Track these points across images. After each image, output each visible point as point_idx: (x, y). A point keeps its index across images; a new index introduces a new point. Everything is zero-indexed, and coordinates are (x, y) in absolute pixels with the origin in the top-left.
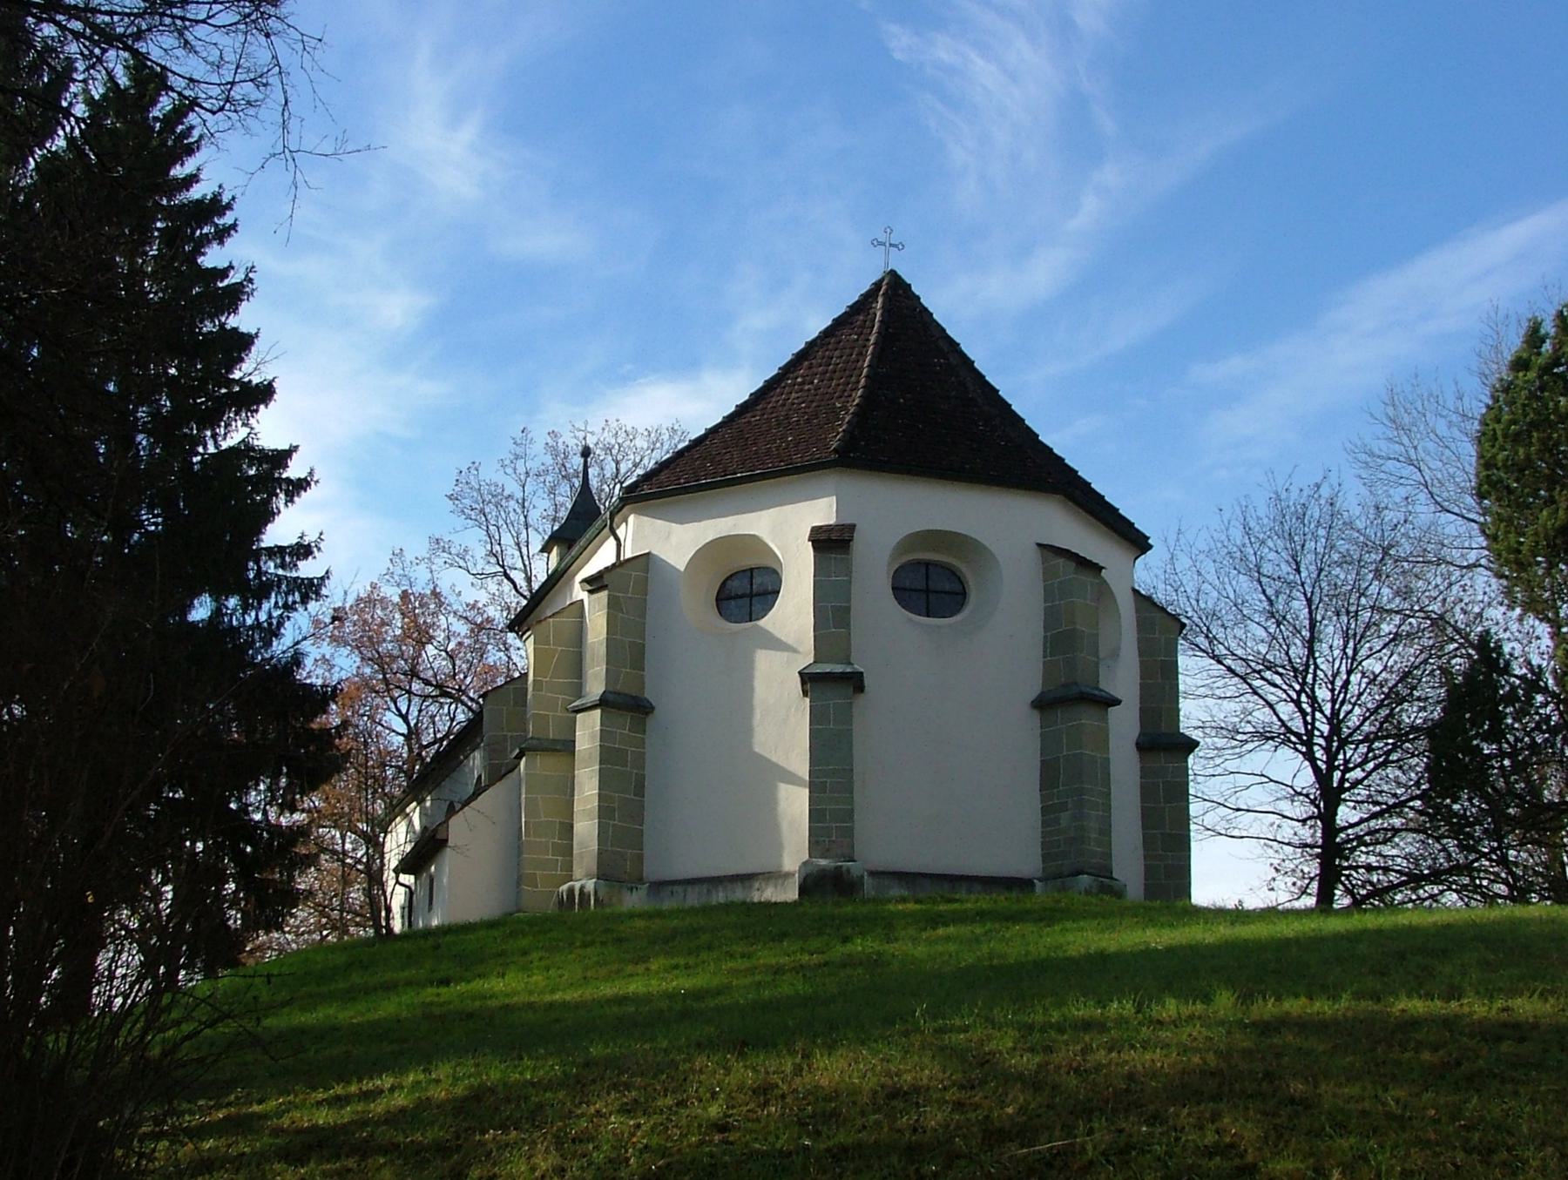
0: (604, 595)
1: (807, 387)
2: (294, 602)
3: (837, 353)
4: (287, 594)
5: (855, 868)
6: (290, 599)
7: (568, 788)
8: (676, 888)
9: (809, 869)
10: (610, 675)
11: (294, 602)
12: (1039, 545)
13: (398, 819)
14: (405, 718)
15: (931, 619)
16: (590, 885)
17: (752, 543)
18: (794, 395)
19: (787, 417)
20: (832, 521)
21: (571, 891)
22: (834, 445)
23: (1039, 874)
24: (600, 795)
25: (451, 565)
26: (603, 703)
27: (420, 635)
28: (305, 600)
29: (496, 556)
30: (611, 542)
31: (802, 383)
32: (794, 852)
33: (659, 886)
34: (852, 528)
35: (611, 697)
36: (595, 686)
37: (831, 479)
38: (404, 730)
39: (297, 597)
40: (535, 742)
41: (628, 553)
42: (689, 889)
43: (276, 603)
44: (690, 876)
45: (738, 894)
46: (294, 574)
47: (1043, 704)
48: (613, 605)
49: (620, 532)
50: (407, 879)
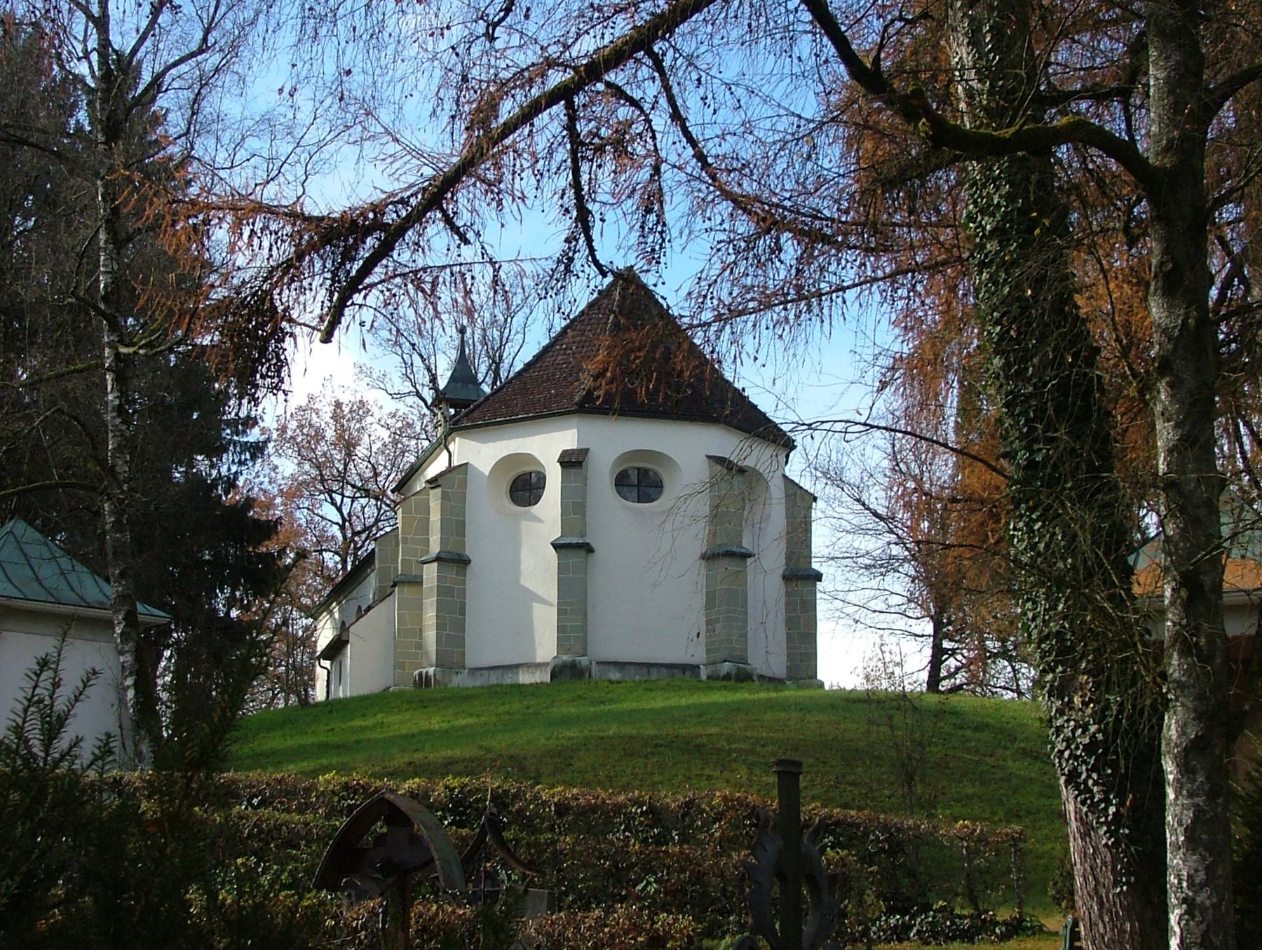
0: (439, 490)
1: (568, 352)
2: (246, 460)
3: (588, 328)
4: (240, 453)
5: (584, 661)
6: (243, 457)
7: (419, 607)
8: (484, 672)
9: (557, 661)
10: (443, 541)
11: (246, 460)
12: (709, 457)
13: (325, 614)
14: (339, 509)
15: (640, 504)
16: (431, 670)
17: (528, 458)
18: (560, 357)
19: (554, 375)
20: (575, 447)
21: (421, 674)
22: (577, 399)
23: (705, 662)
24: (437, 616)
25: (373, 387)
26: (438, 559)
27: (348, 445)
28: (253, 458)
29: (409, 376)
30: (445, 454)
31: (566, 349)
32: (546, 648)
33: (475, 671)
34: (586, 451)
35: (443, 555)
36: (435, 548)
37: (575, 420)
38: (338, 519)
39: (248, 456)
40: (403, 577)
41: (455, 463)
42: (492, 672)
43: (233, 460)
44: (492, 665)
45: (508, 679)
46: (245, 439)
47: (709, 557)
48: (445, 497)
49: (451, 447)
50: (327, 664)
